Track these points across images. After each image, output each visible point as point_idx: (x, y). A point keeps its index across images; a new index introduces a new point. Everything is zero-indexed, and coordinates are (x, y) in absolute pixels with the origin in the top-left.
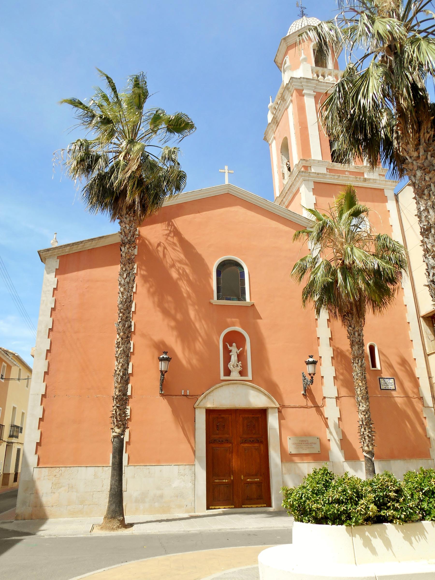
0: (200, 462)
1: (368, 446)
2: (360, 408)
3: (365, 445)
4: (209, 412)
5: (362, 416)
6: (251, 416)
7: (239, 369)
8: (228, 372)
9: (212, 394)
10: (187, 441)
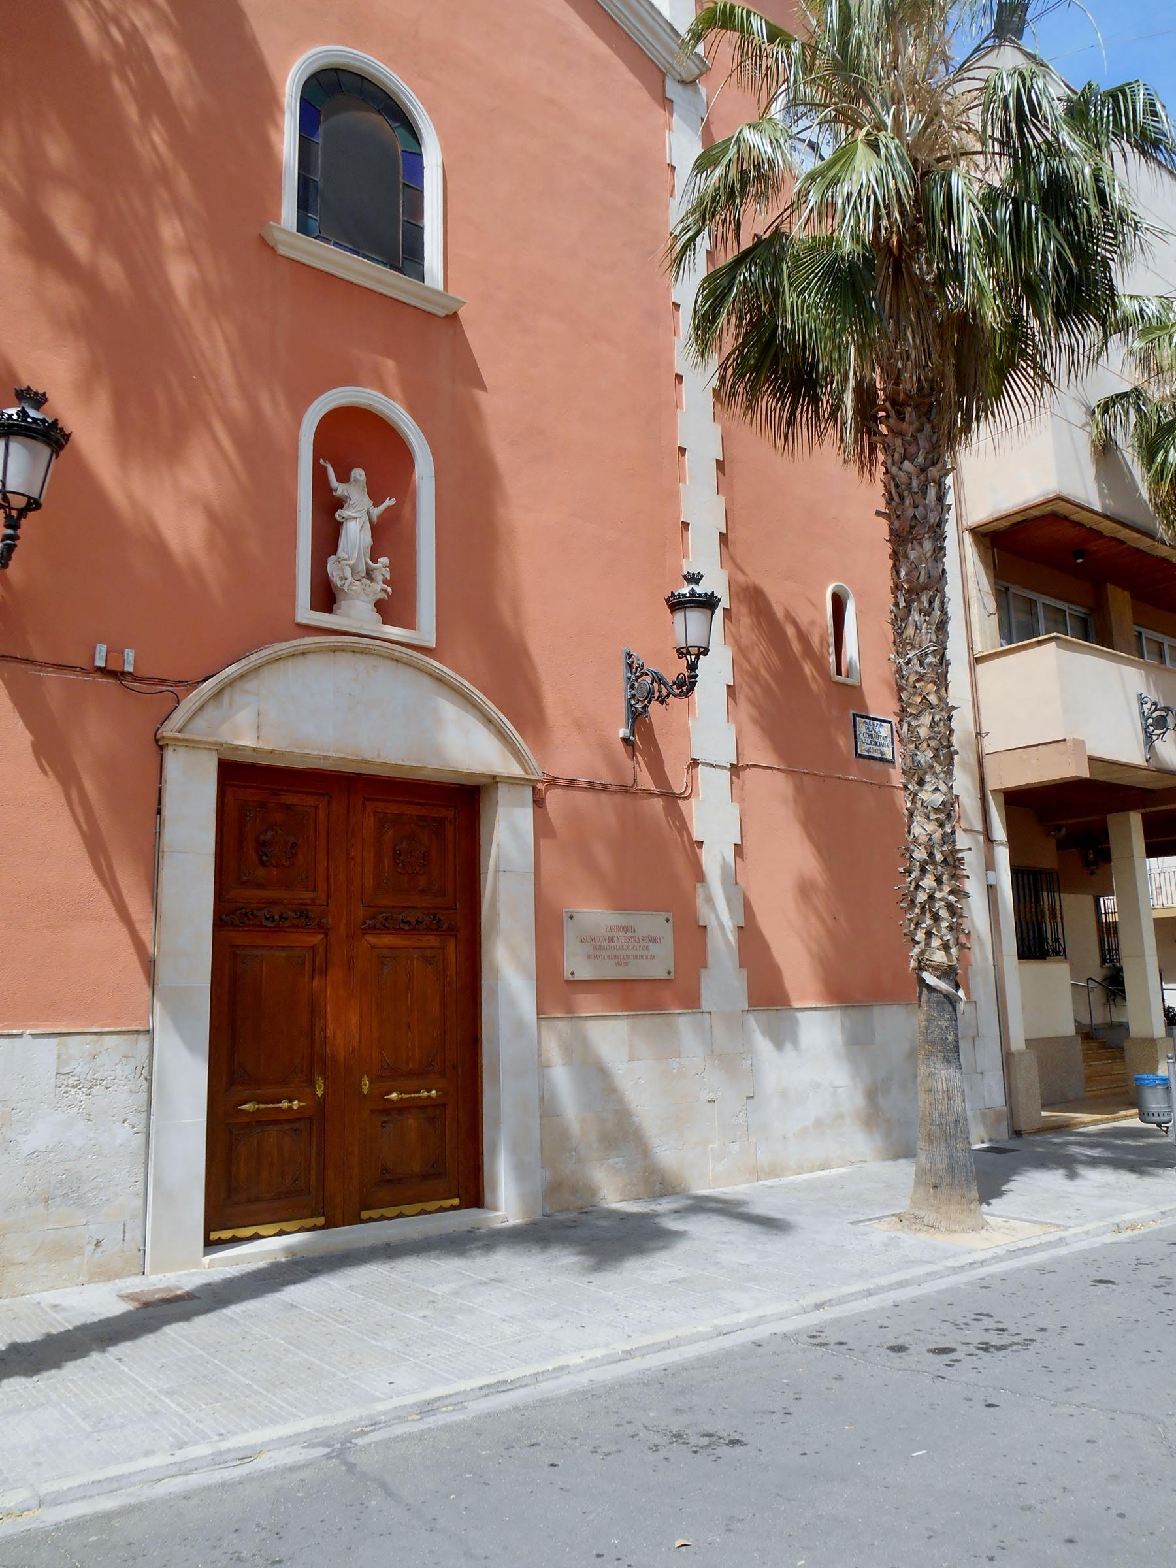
0: (177, 1018)
1: (946, 947)
2: (923, 795)
3: (935, 943)
4: (237, 775)
5: (931, 827)
6: (411, 810)
7: (378, 589)
8: (326, 596)
9: (251, 685)
10: (112, 913)
